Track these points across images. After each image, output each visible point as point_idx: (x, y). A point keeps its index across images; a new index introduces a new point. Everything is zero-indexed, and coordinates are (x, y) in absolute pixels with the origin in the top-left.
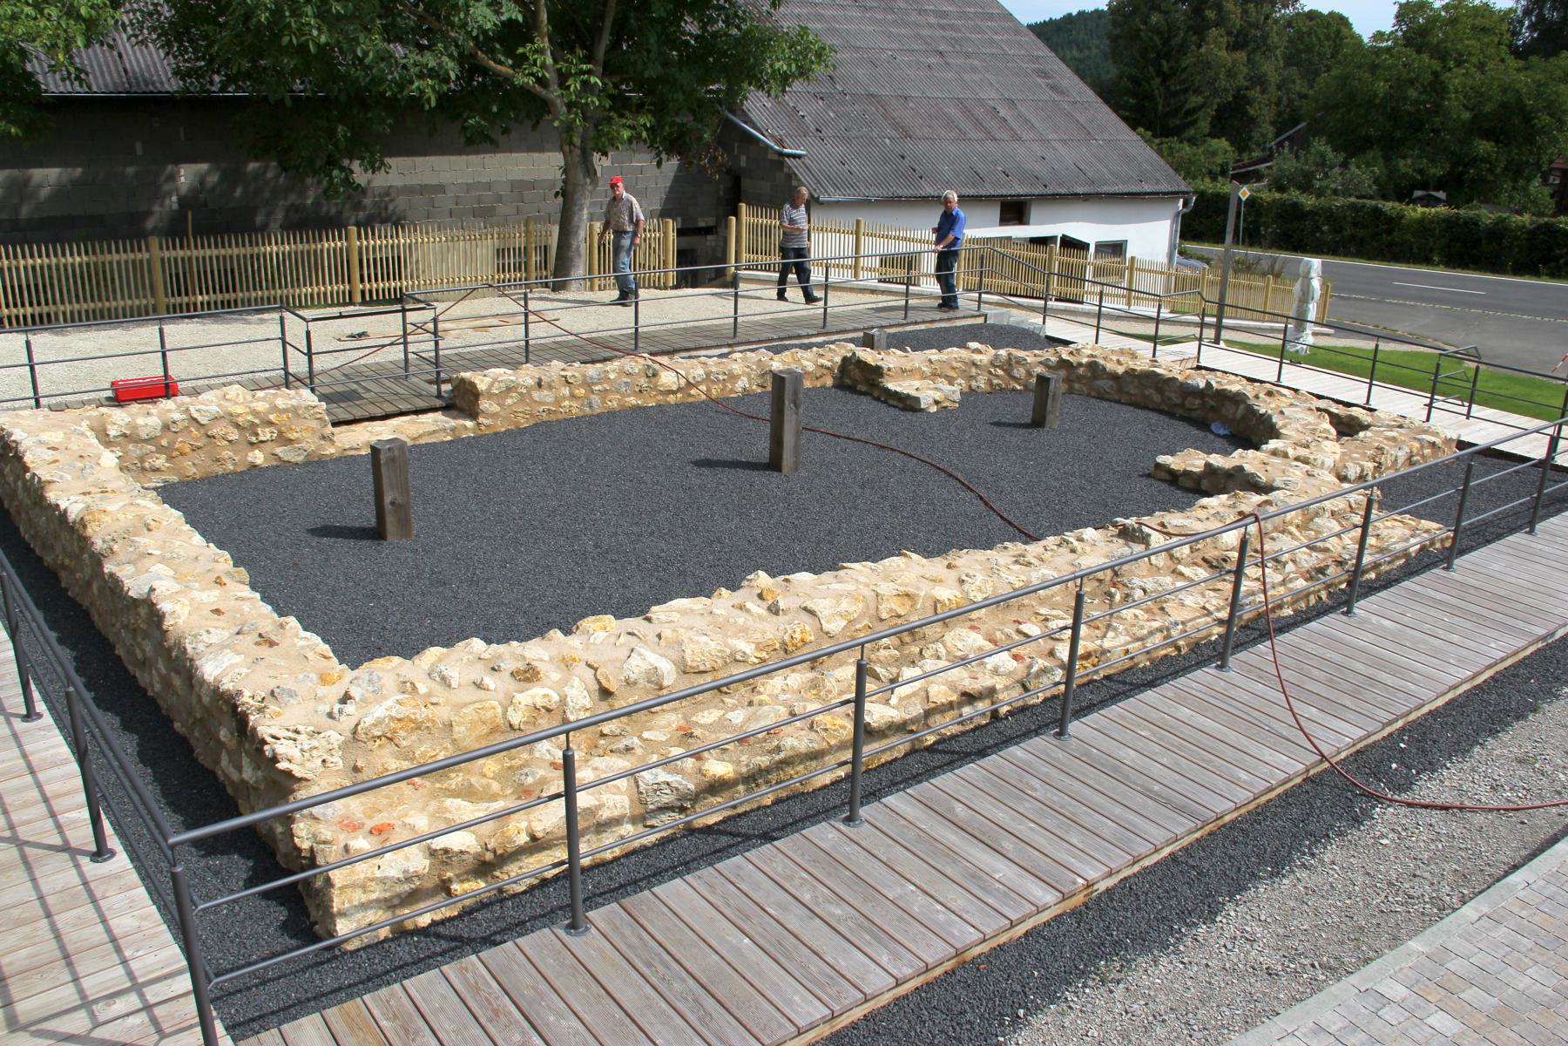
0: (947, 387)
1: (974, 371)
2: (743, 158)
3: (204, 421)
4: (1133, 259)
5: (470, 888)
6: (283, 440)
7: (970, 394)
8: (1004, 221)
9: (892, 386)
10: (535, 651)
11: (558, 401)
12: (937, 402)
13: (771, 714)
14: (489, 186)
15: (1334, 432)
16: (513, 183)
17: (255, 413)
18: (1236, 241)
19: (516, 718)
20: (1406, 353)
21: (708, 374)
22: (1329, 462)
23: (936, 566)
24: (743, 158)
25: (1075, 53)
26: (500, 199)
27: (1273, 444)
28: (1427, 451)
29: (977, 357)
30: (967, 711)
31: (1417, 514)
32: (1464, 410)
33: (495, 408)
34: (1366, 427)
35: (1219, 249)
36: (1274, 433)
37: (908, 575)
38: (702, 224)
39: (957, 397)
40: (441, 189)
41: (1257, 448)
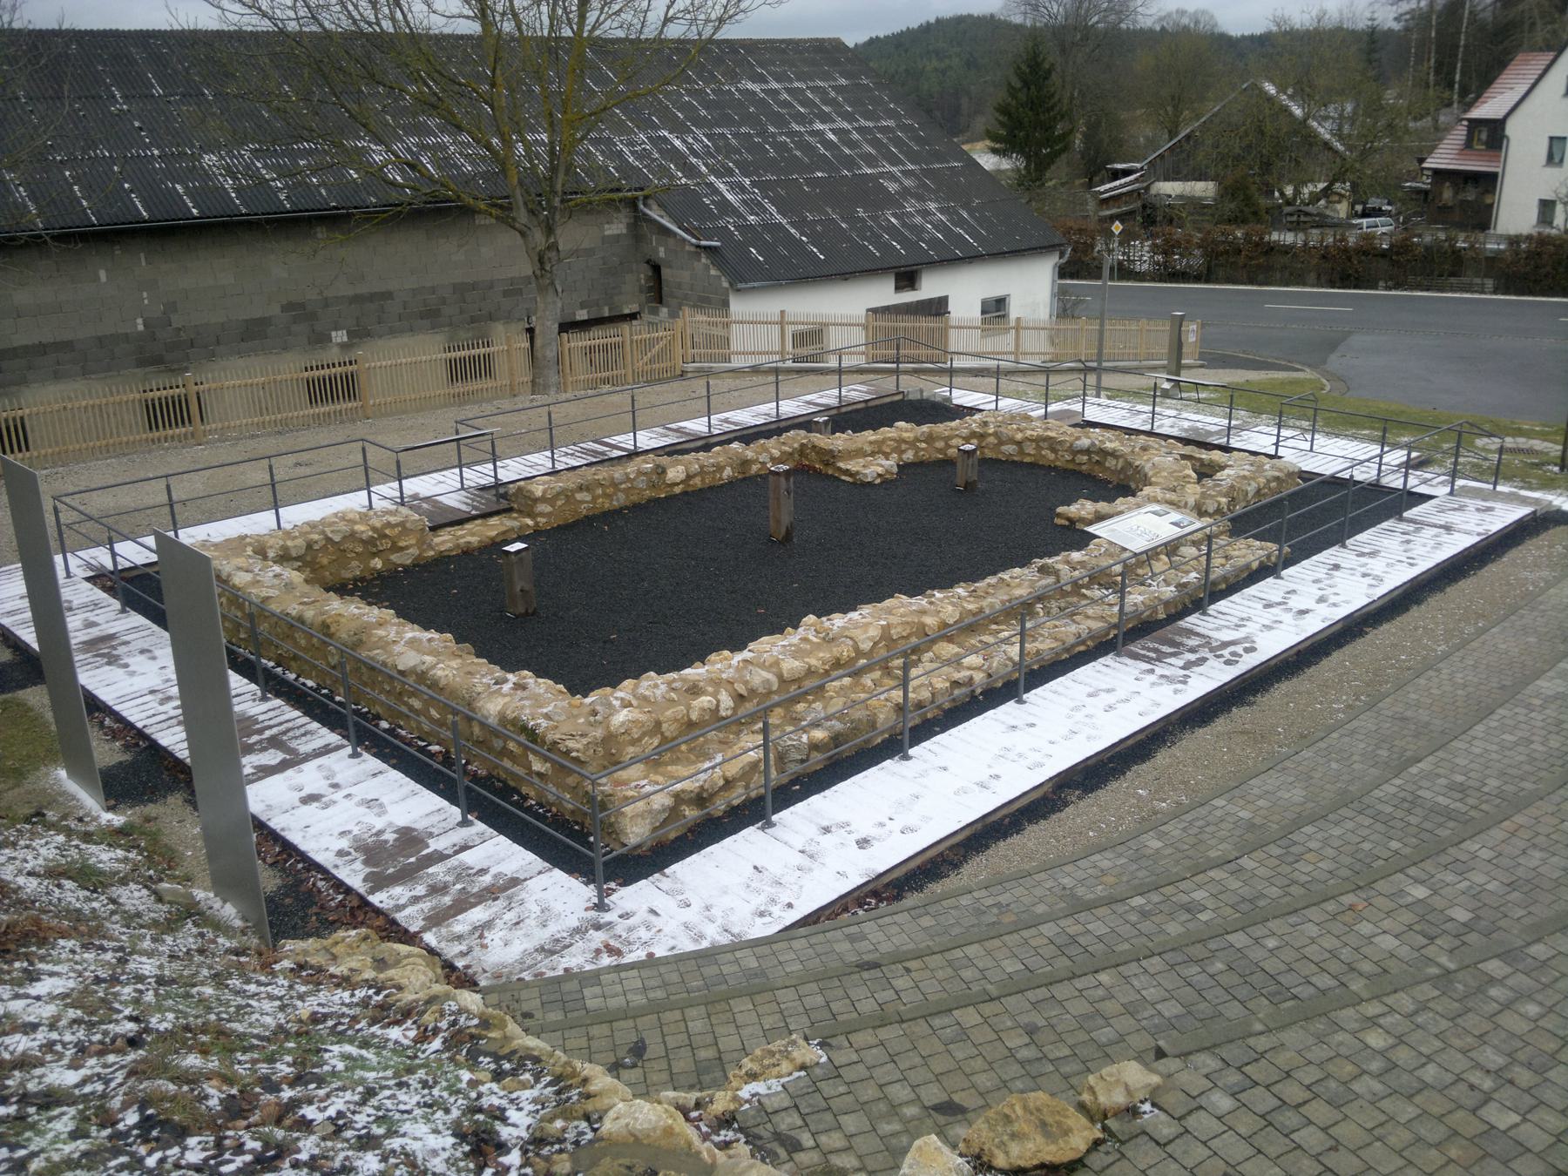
0: (884, 462)
1: (904, 446)
2: (662, 249)
3: (337, 538)
4: (1018, 319)
5: (691, 813)
6: (396, 549)
7: (903, 468)
8: (898, 289)
9: (841, 465)
10: (694, 672)
11: (595, 499)
12: (879, 475)
13: (837, 704)
14: (433, 290)
15: (1194, 475)
16: (454, 285)
17: (374, 529)
18: (1112, 279)
19: (694, 716)
20: (1283, 383)
21: (702, 467)
22: (1191, 501)
23: (920, 602)
24: (662, 249)
25: (935, 63)
26: (444, 301)
27: (1147, 490)
28: (1273, 485)
29: (905, 435)
30: (956, 692)
31: (1256, 537)
32: (1307, 446)
33: (549, 509)
34: (1222, 468)
35: (1099, 283)
36: (1146, 481)
37: (900, 610)
38: (627, 311)
39: (895, 470)
40: (388, 295)
41: (1134, 495)
